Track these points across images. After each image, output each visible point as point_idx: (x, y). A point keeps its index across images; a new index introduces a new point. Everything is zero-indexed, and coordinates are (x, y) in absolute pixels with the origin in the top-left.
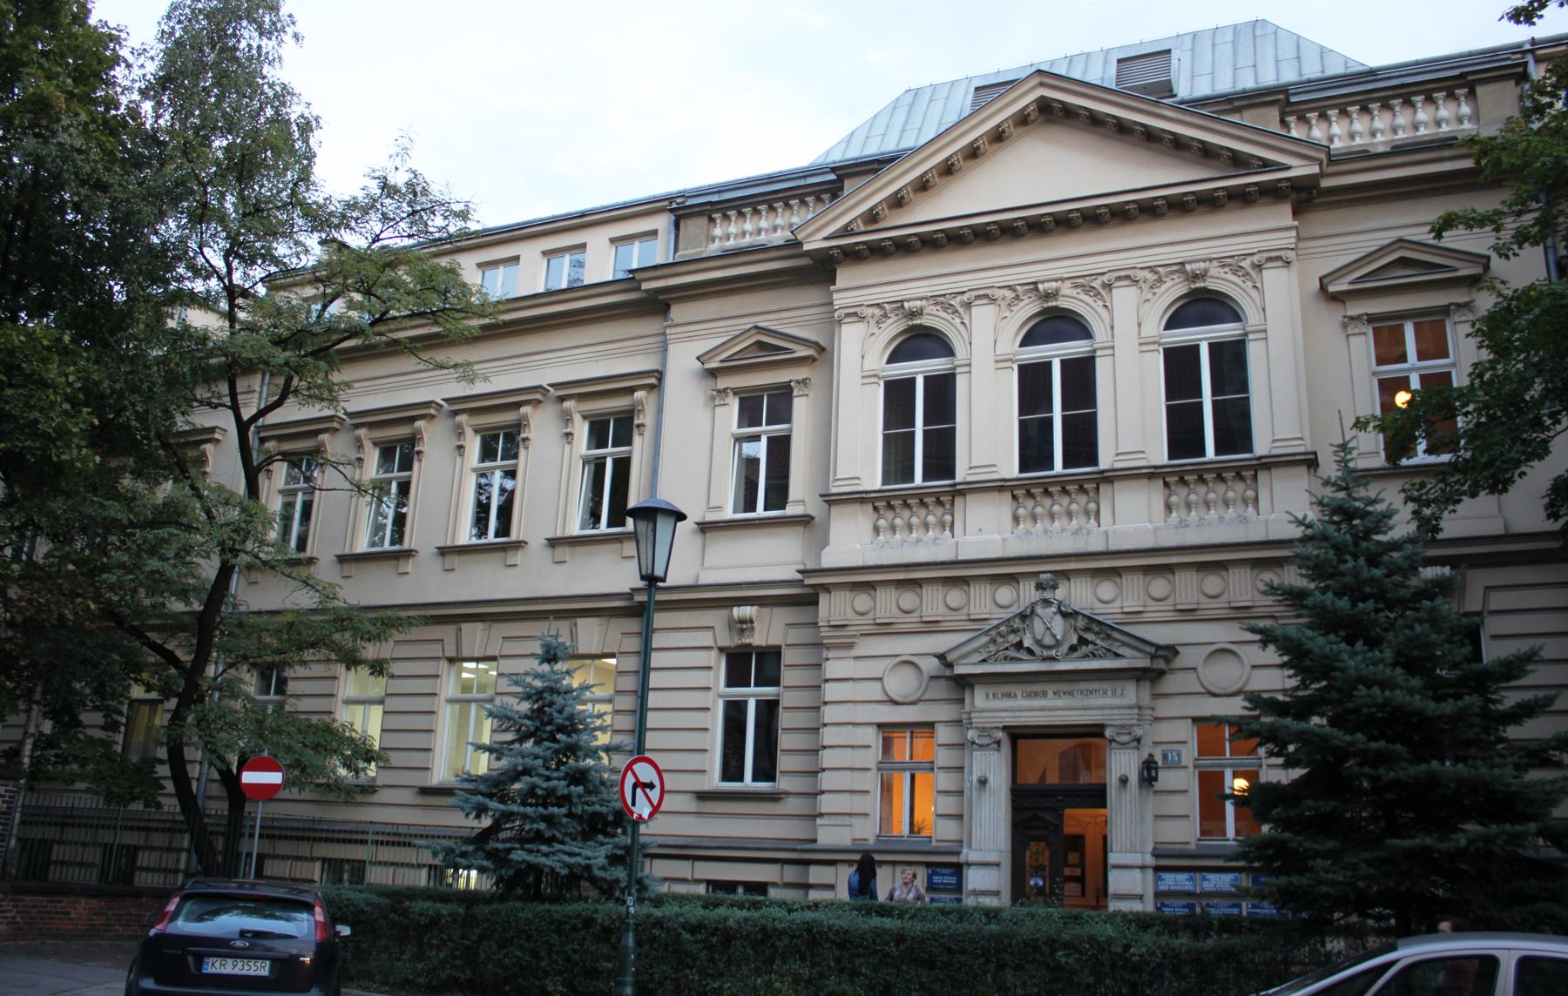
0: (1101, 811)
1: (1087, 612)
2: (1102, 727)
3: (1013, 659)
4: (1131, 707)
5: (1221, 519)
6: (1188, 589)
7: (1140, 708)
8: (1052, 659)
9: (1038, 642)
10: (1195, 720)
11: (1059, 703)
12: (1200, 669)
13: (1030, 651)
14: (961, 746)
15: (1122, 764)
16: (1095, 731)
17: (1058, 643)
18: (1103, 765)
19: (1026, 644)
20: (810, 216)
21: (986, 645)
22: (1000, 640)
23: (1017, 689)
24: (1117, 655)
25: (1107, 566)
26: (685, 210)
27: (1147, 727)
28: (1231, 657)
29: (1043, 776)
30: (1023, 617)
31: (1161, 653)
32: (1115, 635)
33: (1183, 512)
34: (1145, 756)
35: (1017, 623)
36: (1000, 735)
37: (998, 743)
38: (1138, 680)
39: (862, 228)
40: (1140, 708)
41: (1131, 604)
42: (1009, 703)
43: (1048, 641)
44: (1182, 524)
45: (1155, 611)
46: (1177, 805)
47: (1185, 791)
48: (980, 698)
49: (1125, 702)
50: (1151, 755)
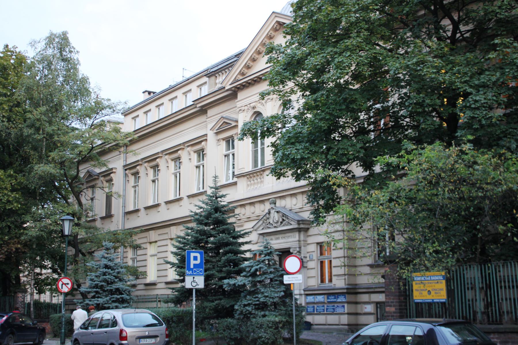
20: (224, 78)
21: (262, 224)
26: (211, 73)
39: (241, 78)
42: (278, 241)
46: (313, 273)
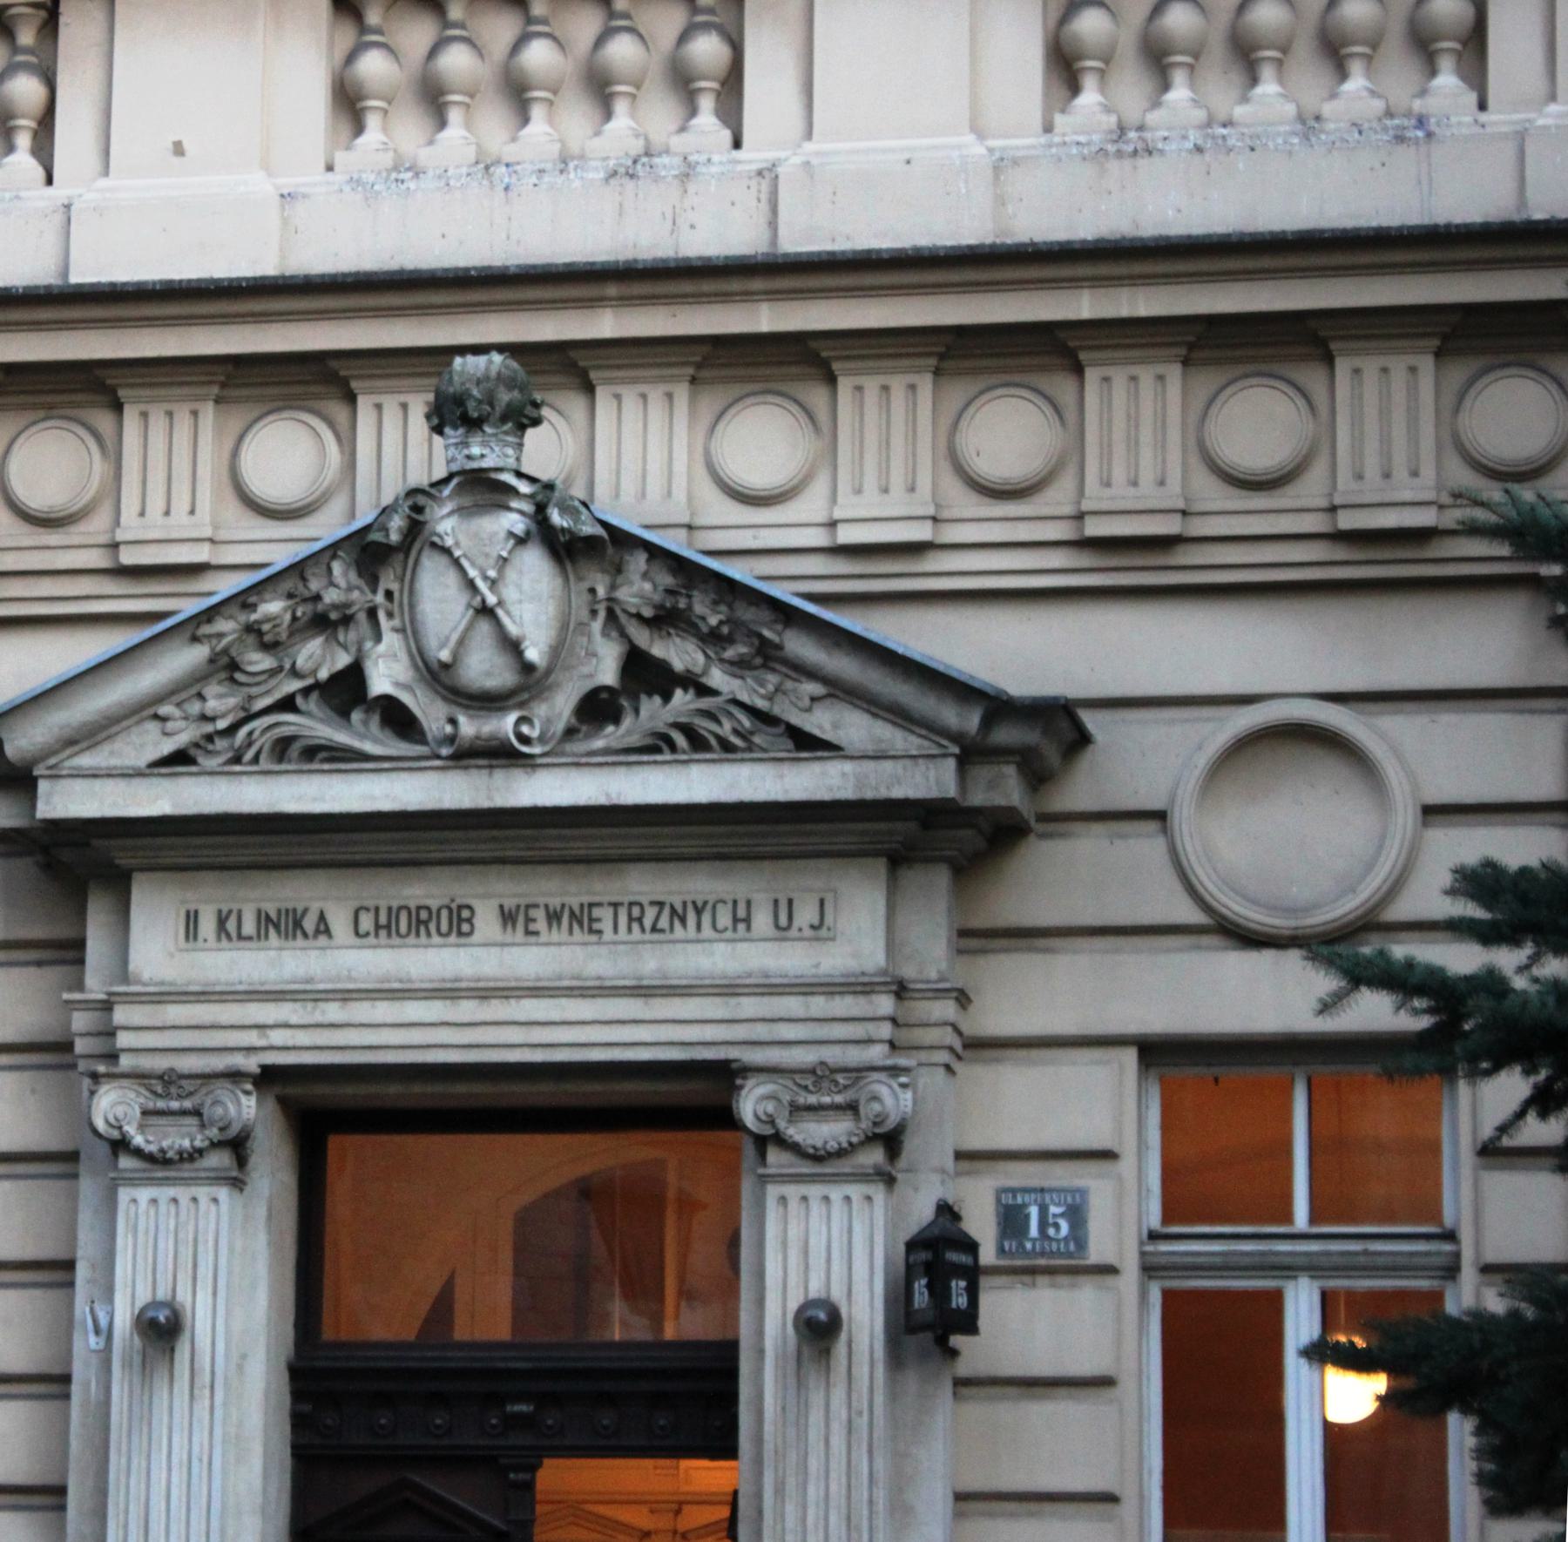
0: (703, 1474)
1: (673, 542)
2: (724, 1075)
3: (320, 756)
4: (860, 986)
5: (1308, 123)
6: (1139, 444)
7: (901, 990)
8: (501, 755)
9: (438, 676)
10: (1157, 1053)
11: (530, 960)
12: (1184, 818)
13: (397, 718)
14: (64, 1162)
15: (818, 1247)
16: (690, 1102)
17: (530, 682)
18: (727, 1271)
19: (381, 682)
21: (189, 687)
22: (260, 662)
23: (331, 896)
24: (806, 744)
25: (763, 327)
27: (932, 1081)
28: (1328, 770)
29: (443, 1307)
30: (370, 553)
31: (1006, 735)
32: (800, 646)
33: (1131, 87)
34: (921, 1212)
35: (340, 585)
36: (246, 1107)
37: (238, 1145)
38: (898, 860)
40: (901, 990)
41: (876, 506)
43: (483, 667)
44: (1128, 143)
45: (985, 541)
47: (1105, 1382)
48: (158, 938)
49: (833, 960)
50: (946, 1211)
